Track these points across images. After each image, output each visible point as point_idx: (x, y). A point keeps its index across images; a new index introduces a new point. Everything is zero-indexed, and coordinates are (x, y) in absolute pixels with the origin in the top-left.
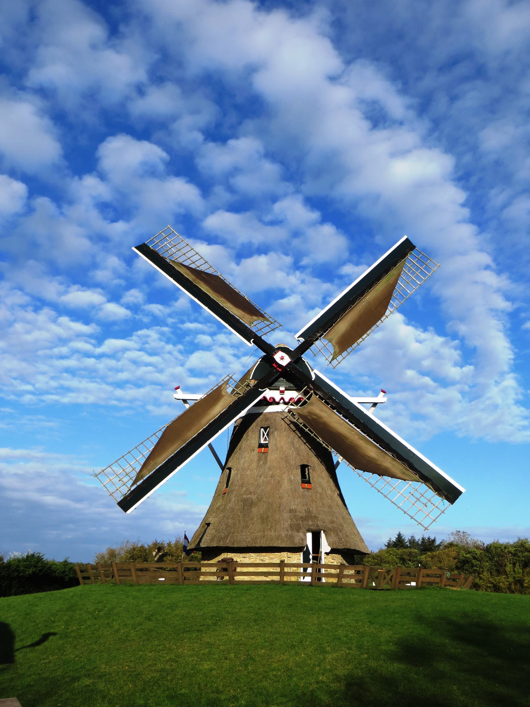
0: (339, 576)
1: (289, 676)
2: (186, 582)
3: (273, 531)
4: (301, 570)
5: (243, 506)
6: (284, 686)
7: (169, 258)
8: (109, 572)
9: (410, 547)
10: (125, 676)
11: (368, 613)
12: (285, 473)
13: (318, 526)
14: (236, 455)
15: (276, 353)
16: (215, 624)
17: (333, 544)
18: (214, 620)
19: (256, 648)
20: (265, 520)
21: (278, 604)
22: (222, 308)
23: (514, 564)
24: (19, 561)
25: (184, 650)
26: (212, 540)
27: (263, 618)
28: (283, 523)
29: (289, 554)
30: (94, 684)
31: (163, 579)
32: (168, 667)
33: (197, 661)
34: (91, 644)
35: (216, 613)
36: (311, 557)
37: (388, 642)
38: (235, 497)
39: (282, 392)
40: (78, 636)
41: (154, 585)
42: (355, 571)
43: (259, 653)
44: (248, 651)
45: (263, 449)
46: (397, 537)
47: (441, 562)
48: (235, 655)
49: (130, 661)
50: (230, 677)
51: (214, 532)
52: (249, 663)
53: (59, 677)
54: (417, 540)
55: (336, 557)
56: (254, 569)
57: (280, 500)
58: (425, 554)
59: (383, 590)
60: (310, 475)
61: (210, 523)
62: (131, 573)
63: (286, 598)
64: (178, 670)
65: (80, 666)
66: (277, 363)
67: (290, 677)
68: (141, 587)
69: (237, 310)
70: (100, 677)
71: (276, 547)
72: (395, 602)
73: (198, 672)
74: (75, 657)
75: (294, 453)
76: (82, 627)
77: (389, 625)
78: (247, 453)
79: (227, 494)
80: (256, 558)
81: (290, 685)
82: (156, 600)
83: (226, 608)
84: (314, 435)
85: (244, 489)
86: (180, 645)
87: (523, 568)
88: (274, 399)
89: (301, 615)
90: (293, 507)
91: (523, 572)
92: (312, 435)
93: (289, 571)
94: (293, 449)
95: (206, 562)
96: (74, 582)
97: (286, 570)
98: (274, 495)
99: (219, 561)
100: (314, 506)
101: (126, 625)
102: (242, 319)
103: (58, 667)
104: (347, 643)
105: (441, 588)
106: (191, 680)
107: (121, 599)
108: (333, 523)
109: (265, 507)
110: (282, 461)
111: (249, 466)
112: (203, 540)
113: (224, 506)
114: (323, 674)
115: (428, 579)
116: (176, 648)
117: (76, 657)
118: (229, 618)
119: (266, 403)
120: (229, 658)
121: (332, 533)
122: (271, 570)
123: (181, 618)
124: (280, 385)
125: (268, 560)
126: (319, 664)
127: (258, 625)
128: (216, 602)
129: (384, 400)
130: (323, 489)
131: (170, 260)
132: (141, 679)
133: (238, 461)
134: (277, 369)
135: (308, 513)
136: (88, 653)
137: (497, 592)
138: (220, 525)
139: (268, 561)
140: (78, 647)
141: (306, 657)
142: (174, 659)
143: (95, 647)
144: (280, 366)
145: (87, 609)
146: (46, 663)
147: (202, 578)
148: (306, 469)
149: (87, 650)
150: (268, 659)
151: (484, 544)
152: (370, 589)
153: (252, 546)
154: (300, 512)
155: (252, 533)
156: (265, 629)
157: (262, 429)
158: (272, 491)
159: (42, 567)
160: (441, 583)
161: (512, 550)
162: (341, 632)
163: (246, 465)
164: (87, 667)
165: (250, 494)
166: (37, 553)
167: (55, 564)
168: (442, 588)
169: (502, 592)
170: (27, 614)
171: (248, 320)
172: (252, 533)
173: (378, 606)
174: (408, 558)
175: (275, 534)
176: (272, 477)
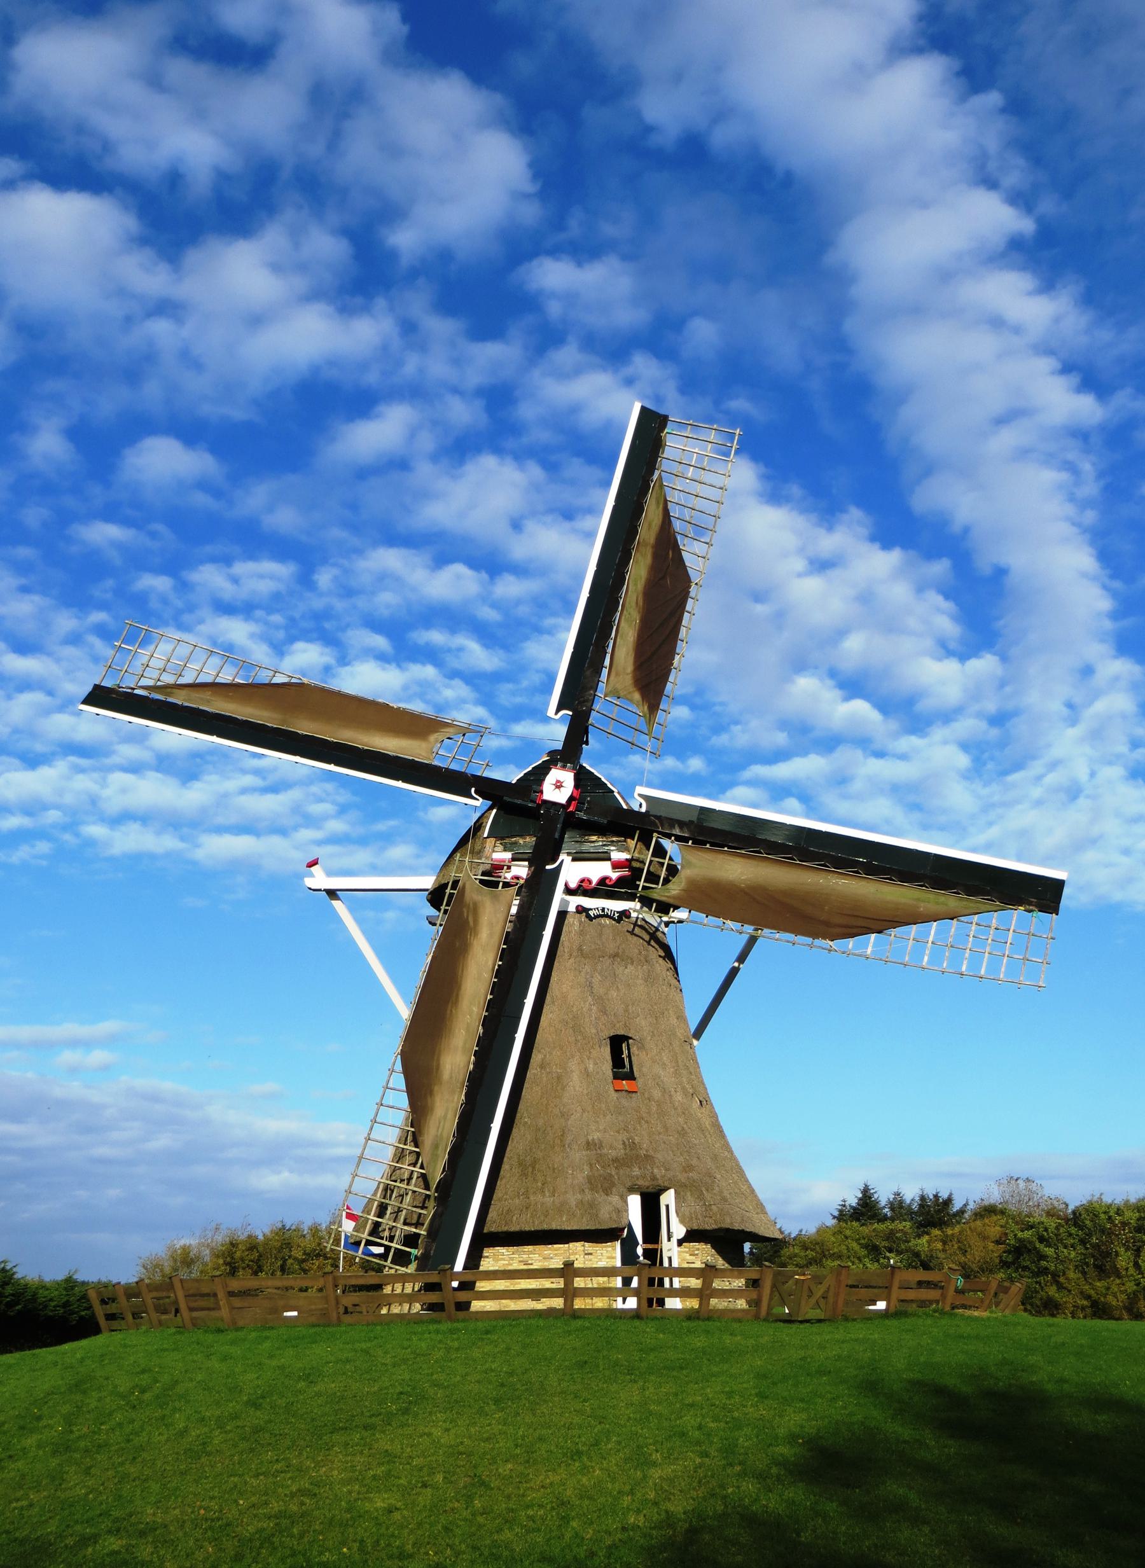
0: (704, 1294)
1: (563, 1517)
2: (347, 1319)
4: (618, 1282)
6: (548, 1540)
9: (893, 1219)
10: (198, 1529)
11: (761, 1376)
12: (573, 1057)
13: (654, 1178)
16: (406, 1411)
18: (403, 1403)
19: (493, 1461)
20: (530, 1169)
21: (554, 1362)
25: (332, 1469)
27: (517, 1393)
29: (589, 1247)
30: (128, 1548)
31: (295, 1313)
32: (294, 1508)
33: (359, 1493)
34: (122, 1464)
36: (640, 1251)
37: (792, 1438)
40: (94, 1447)
43: (500, 1470)
44: (475, 1467)
46: (860, 1195)
47: (966, 1251)
48: (445, 1478)
49: (210, 1497)
50: (432, 1525)
52: (476, 1493)
53: (52, 1538)
55: (698, 1249)
56: (508, 1284)
57: (562, 1120)
59: (807, 1321)
60: (633, 1058)
62: (217, 1303)
63: (575, 1349)
64: (316, 1513)
65: (98, 1512)
67: (566, 1520)
68: (241, 1334)
70: (142, 1534)
73: (360, 1516)
74: (87, 1494)
75: (594, 1008)
76: (103, 1427)
77: (802, 1400)
80: (512, 1259)
81: (561, 1537)
82: (274, 1363)
83: (432, 1374)
86: (322, 1460)
89: (605, 1386)
90: (596, 1136)
93: (590, 1286)
96: (87, 1328)
97: (579, 1282)
98: (550, 1110)
100: (643, 1132)
101: (203, 1419)
103: (50, 1515)
104: (698, 1443)
105: (943, 1313)
106: (343, 1534)
109: (529, 1137)
114: (638, 1511)
115: (911, 1295)
116: (315, 1467)
117: (91, 1492)
118: (439, 1395)
120: (432, 1485)
121: (689, 1194)
122: (547, 1284)
123: (329, 1400)
126: (631, 1490)
127: (503, 1409)
128: (410, 1363)
132: (234, 1535)
137: (1101, 1318)
139: (540, 1264)
140: (93, 1471)
142: (309, 1490)
143: (132, 1470)
145: (116, 1387)
146: (22, 1508)
149: (115, 1477)
150: (520, 1482)
151: (1067, 1205)
152: (776, 1321)
153: (500, 1230)
154: (611, 1147)
158: (544, 1101)
159: (13, 1295)
160: (944, 1303)
162: (689, 1420)
164: (116, 1513)
167: (44, 1287)
168: (945, 1313)
169: (1112, 1318)
173: (784, 1359)
175: (553, 1202)
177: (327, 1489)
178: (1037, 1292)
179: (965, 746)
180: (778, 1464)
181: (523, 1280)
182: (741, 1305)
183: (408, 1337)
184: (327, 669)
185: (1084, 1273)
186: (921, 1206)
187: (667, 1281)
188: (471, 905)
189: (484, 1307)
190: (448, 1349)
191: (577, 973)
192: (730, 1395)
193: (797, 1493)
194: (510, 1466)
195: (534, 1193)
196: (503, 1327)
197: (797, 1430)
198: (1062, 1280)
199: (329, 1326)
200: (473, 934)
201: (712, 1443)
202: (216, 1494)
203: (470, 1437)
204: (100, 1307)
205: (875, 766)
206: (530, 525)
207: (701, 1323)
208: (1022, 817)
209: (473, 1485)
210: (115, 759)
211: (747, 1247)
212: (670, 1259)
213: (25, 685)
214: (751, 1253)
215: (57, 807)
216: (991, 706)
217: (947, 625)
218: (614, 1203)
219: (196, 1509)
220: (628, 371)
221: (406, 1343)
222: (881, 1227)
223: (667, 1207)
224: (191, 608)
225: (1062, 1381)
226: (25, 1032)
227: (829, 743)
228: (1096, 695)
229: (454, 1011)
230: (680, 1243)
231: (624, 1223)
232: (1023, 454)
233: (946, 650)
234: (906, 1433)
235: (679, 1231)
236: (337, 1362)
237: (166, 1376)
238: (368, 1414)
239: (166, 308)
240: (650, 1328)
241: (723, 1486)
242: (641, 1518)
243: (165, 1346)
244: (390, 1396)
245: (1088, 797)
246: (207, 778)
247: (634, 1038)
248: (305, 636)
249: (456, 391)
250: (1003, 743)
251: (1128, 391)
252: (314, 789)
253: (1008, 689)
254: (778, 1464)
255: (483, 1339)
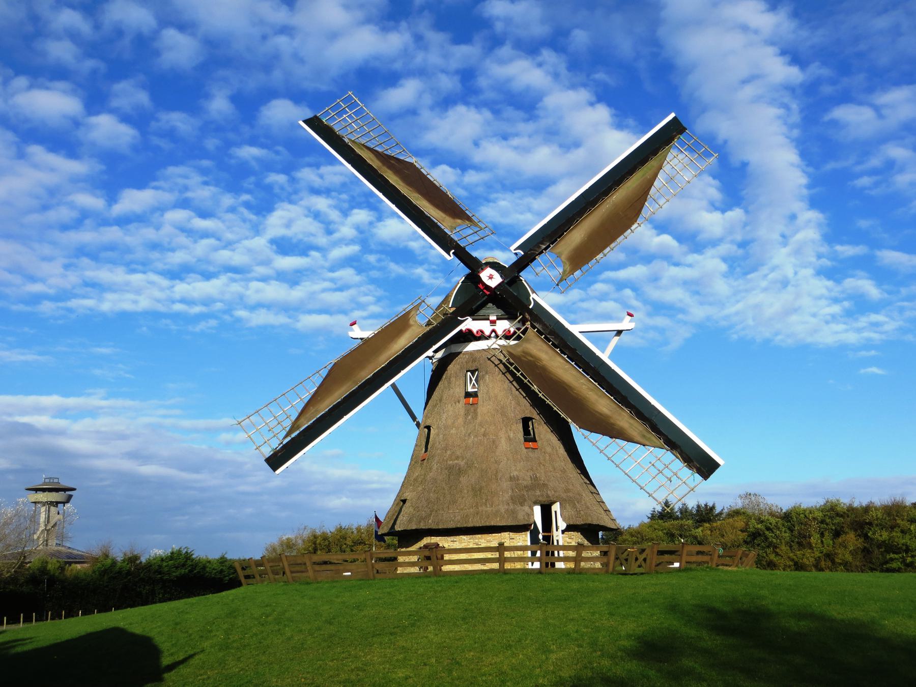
0: (577, 560)
3: (488, 506)
4: (529, 554)
5: (449, 475)
7: (348, 136)
8: (279, 567)
9: (682, 519)
11: (610, 603)
13: (548, 496)
14: (436, 409)
15: (483, 270)
16: (413, 625)
17: (569, 519)
20: (479, 492)
22: (416, 208)
23: (822, 535)
24: (162, 560)
25: (374, 656)
26: (410, 521)
28: (502, 495)
31: (350, 574)
32: (353, 677)
33: (389, 669)
34: (258, 655)
35: (414, 611)
36: (541, 537)
37: (629, 636)
38: (437, 465)
39: (493, 323)
41: (337, 581)
42: (601, 552)
43: (467, 656)
44: (452, 654)
45: (471, 399)
48: (436, 660)
51: (412, 510)
52: (454, 668)
54: (690, 509)
55: (573, 536)
56: (467, 556)
57: (496, 465)
58: (701, 526)
59: (635, 574)
60: (535, 430)
61: (406, 500)
63: (506, 590)
64: (366, 680)
65: (246, 681)
66: (484, 284)
69: (435, 211)
71: (494, 526)
72: (646, 588)
73: (390, 681)
74: (239, 671)
75: (513, 402)
76: (246, 636)
77: (634, 616)
78: (450, 405)
79: (426, 460)
82: (339, 600)
83: (427, 605)
84: (528, 381)
85: (449, 452)
87: (834, 538)
88: (482, 331)
89: (523, 610)
90: (515, 473)
91: (834, 543)
92: (526, 381)
93: (513, 556)
94: (511, 397)
95: (404, 550)
96: (235, 583)
97: (507, 554)
98: (489, 459)
99: (421, 548)
101: (301, 631)
102: (442, 222)
103: (220, 682)
104: (576, 640)
105: (711, 569)
107: (294, 600)
108: (568, 492)
110: (497, 414)
111: (454, 423)
112: (398, 522)
113: (423, 477)
116: (364, 655)
119: (468, 337)
121: (567, 505)
122: (489, 555)
124: (490, 313)
125: (485, 543)
126: (540, 665)
129: (631, 326)
130: (553, 448)
131: (349, 139)
133: (438, 417)
134: (483, 292)
135: (535, 481)
136: (255, 666)
138: (420, 501)
141: (525, 658)
142: (361, 668)
143: (264, 658)
144: (487, 287)
146: (204, 679)
147: (400, 570)
148: (530, 423)
150: (478, 662)
151: (782, 510)
152: (618, 574)
153: (462, 526)
154: (524, 480)
155: (462, 509)
156: (476, 628)
157: (469, 373)
158: (486, 455)
161: (819, 515)
162: (571, 628)
163: (450, 422)
165: (457, 459)
166: (183, 548)
167: (209, 562)
168: (713, 569)
169: (806, 570)
170: (177, 624)
171: (450, 224)
172: (462, 509)
173: (623, 595)
174: (678, 532)
175: (492, 510)
176: (484, 435)
177: (372, 667)
178: (765, 557)
179: (724, 259)
180: (620, 650)
181: (476, 554)
182: (598, 566)
183: (413, 585)
184: (371, 223)
185: (791, 547)
186: (698, 511)
187: (556, 553)
188: (523, 354)
189: (454, 569)
190: (435, 592)
191: (503, 382)
192: (593, 614)
193: (633, 666)
194: (472, 653)
195: (481, 506)
196: (465, 579)
197: (631, 632)
198: (778, 550)
199: (368, 580)
200: (539, 361)
201: (584, 640)
202: (310, 670)
203: (449, 638)
204: (242, 572)
205: (674, 271)
206: (484, 144)
207: (576, 576)
208: (756, 298)
209: (452, 664)
210: (253, 275)
211: (600, 533)
212: (558, 541)
213: (205, 235)
214: (602, 538)
215: (221, 301)
216: (739, 237)
217: (714, 193)
218: (526, 510)
219: (300, 678)
220: (540, 59)
221: (412, 589)
222: (676, 522)
223: (556, 512)
224: (296, 192)
225: (780, 604)
226: (201, 423)
227: (648, 259)
228: (797, 231)
229: (575, 392)
230: (563, 532)
231: (531, 521)
232: (757, 99)
233: (713, 206)
234: (693, 633)
235: (562, 525)
236: (374, 599)
237: (280, 608)
238: (393, 627)
239: (286, 30)
240: (547, 579)
241: (590, 663)
242: (546, 680)
243: (278, 592)
244: (404, 617)
245: (793, 286)
246: (304, 284)
247: (535, 418)
248: (359, 206)
249: (443, 71)
250: (746, 257)
251: (817, 64)
252: (362, 289)
253: (748, 228)
254: (620, 650)
255: (454, 586)
